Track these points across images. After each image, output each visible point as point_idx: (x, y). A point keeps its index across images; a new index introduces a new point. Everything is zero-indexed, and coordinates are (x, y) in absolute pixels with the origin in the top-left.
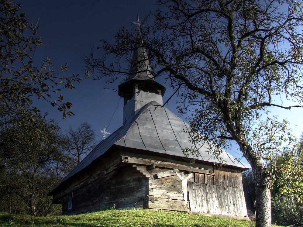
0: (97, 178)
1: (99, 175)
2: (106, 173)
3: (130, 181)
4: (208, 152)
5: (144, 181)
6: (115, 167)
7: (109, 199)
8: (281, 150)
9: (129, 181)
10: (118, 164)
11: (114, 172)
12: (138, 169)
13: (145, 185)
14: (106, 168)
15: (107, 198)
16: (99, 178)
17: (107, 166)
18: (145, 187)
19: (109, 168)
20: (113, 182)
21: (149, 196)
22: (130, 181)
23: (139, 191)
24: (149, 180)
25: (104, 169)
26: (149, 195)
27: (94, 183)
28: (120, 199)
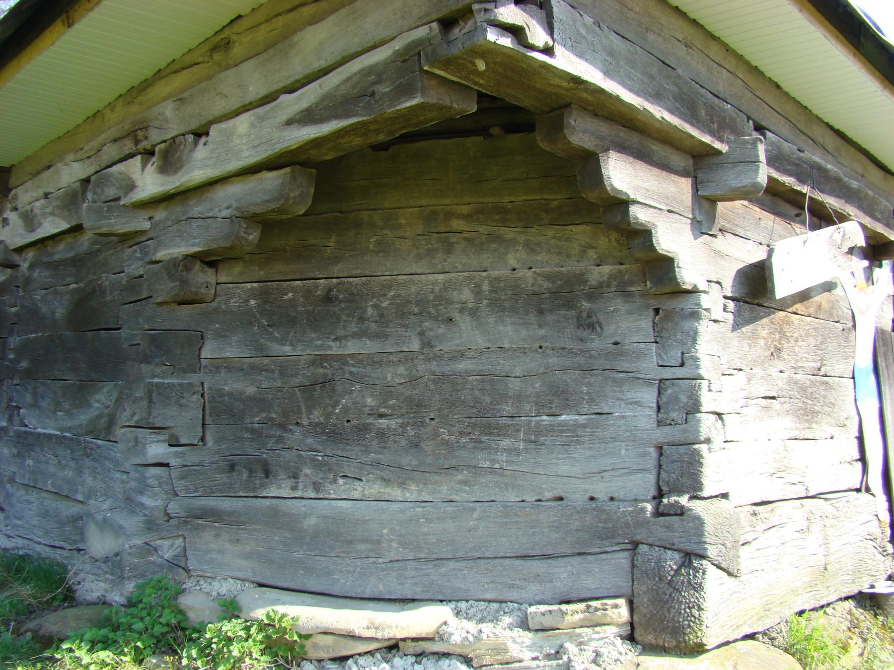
0: (50, 227)
1: (73, 199)
2: (149, 182)
3: (442, 299)
4: (218, 284)
5: (629, 325)
6: (308, 117)
7: (187, 471)
8: (159, 626)
9: (435, 309)
10: (370, 70)
11: (271, 180)
12: (621, 174)
13: (649, 366)
14: (155, 136)
15: (157, 449)
16: (77, 229)
17: (168, 110)
18: (649, 396)
19: (200, 133)
20: (235, 288)
21: (697, 507)
22: (442, 299)
23: (571, 437)
24: (695, 316)
25: (128, 146)
26: (695, 489)
27: (25, 265)
28: (316, 486)
